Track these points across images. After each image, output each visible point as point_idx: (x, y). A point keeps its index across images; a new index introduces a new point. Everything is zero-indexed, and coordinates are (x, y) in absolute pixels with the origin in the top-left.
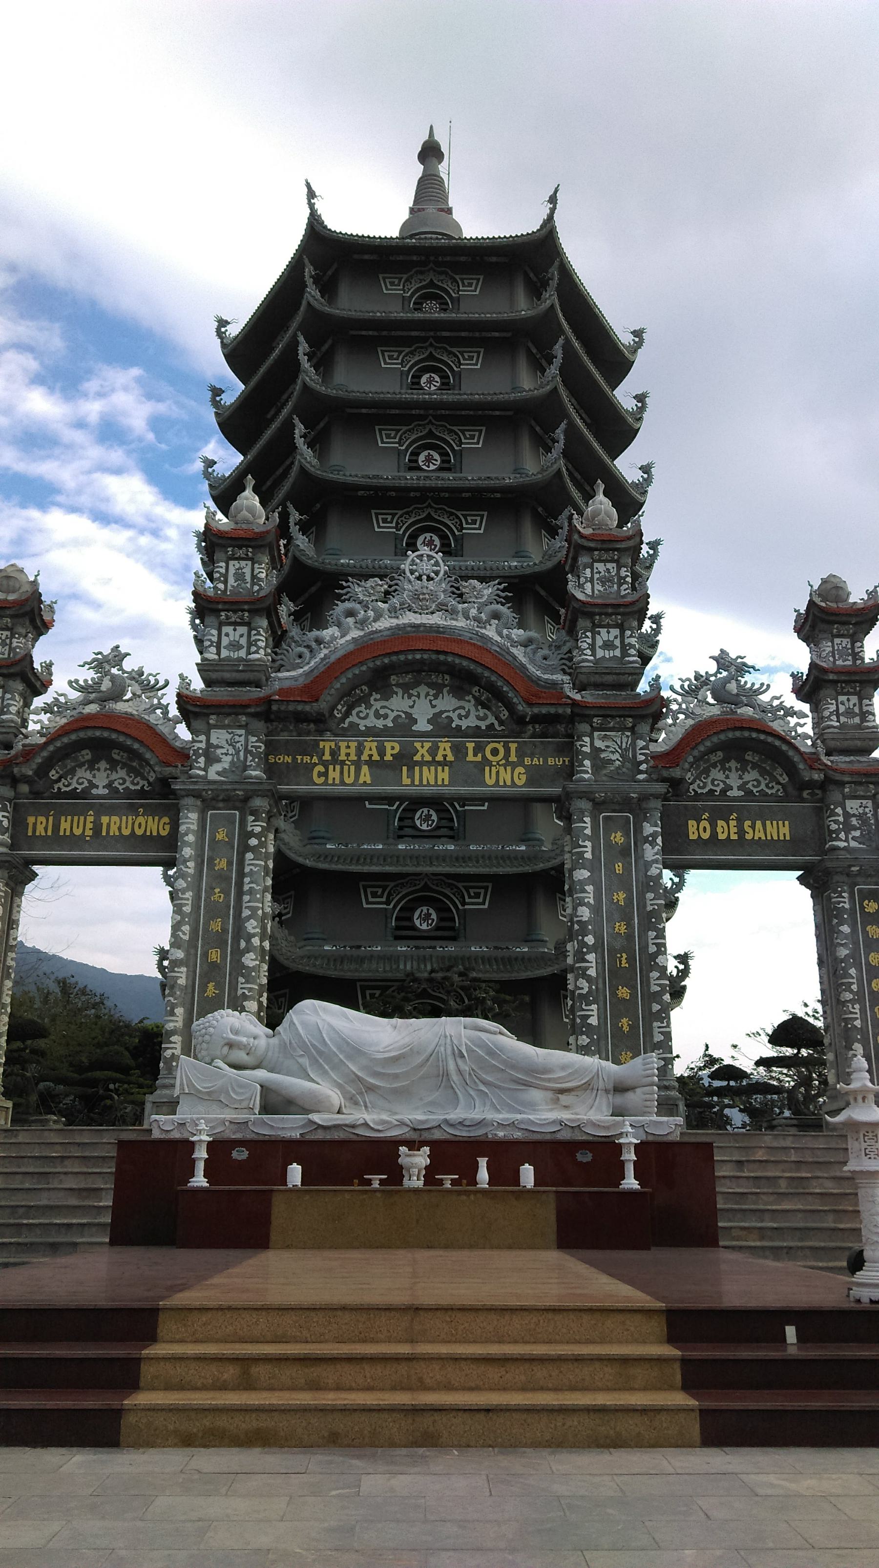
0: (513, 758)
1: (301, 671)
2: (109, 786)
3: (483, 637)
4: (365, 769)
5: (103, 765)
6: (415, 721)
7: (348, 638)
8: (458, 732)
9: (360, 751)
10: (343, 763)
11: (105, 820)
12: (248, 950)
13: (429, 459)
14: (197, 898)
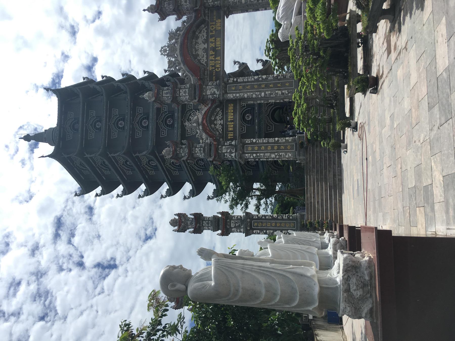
0: (214, 23)
1: (191, 78)
2: (220, 120)
3: (183, 34)
4: (217, 58)
5: (215, 122)
6: (205, 48)
7: (183, 67)
9: (212, 60)
10: (215, 64)
11: (229, 120)
12: (262, 78)
13: (121, 124)
14: (249, 92)
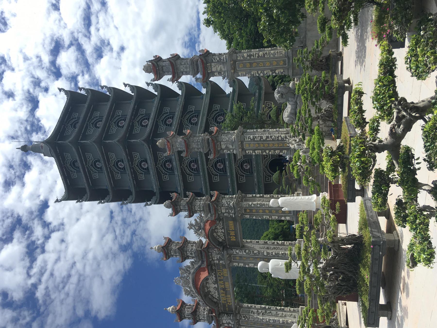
3: (193, 273)
8: (216, 280)
